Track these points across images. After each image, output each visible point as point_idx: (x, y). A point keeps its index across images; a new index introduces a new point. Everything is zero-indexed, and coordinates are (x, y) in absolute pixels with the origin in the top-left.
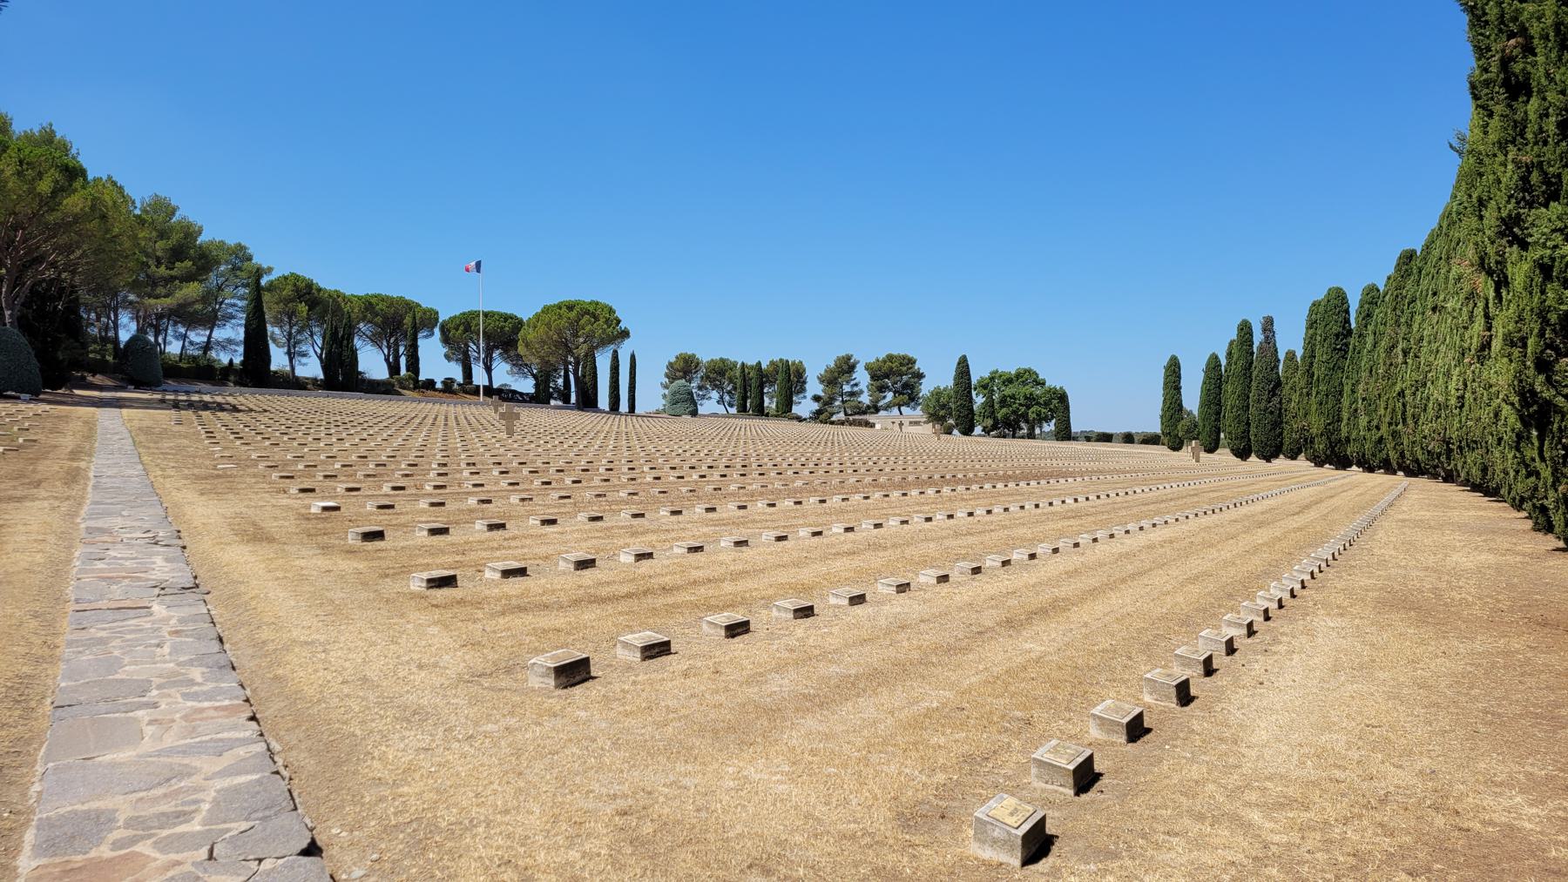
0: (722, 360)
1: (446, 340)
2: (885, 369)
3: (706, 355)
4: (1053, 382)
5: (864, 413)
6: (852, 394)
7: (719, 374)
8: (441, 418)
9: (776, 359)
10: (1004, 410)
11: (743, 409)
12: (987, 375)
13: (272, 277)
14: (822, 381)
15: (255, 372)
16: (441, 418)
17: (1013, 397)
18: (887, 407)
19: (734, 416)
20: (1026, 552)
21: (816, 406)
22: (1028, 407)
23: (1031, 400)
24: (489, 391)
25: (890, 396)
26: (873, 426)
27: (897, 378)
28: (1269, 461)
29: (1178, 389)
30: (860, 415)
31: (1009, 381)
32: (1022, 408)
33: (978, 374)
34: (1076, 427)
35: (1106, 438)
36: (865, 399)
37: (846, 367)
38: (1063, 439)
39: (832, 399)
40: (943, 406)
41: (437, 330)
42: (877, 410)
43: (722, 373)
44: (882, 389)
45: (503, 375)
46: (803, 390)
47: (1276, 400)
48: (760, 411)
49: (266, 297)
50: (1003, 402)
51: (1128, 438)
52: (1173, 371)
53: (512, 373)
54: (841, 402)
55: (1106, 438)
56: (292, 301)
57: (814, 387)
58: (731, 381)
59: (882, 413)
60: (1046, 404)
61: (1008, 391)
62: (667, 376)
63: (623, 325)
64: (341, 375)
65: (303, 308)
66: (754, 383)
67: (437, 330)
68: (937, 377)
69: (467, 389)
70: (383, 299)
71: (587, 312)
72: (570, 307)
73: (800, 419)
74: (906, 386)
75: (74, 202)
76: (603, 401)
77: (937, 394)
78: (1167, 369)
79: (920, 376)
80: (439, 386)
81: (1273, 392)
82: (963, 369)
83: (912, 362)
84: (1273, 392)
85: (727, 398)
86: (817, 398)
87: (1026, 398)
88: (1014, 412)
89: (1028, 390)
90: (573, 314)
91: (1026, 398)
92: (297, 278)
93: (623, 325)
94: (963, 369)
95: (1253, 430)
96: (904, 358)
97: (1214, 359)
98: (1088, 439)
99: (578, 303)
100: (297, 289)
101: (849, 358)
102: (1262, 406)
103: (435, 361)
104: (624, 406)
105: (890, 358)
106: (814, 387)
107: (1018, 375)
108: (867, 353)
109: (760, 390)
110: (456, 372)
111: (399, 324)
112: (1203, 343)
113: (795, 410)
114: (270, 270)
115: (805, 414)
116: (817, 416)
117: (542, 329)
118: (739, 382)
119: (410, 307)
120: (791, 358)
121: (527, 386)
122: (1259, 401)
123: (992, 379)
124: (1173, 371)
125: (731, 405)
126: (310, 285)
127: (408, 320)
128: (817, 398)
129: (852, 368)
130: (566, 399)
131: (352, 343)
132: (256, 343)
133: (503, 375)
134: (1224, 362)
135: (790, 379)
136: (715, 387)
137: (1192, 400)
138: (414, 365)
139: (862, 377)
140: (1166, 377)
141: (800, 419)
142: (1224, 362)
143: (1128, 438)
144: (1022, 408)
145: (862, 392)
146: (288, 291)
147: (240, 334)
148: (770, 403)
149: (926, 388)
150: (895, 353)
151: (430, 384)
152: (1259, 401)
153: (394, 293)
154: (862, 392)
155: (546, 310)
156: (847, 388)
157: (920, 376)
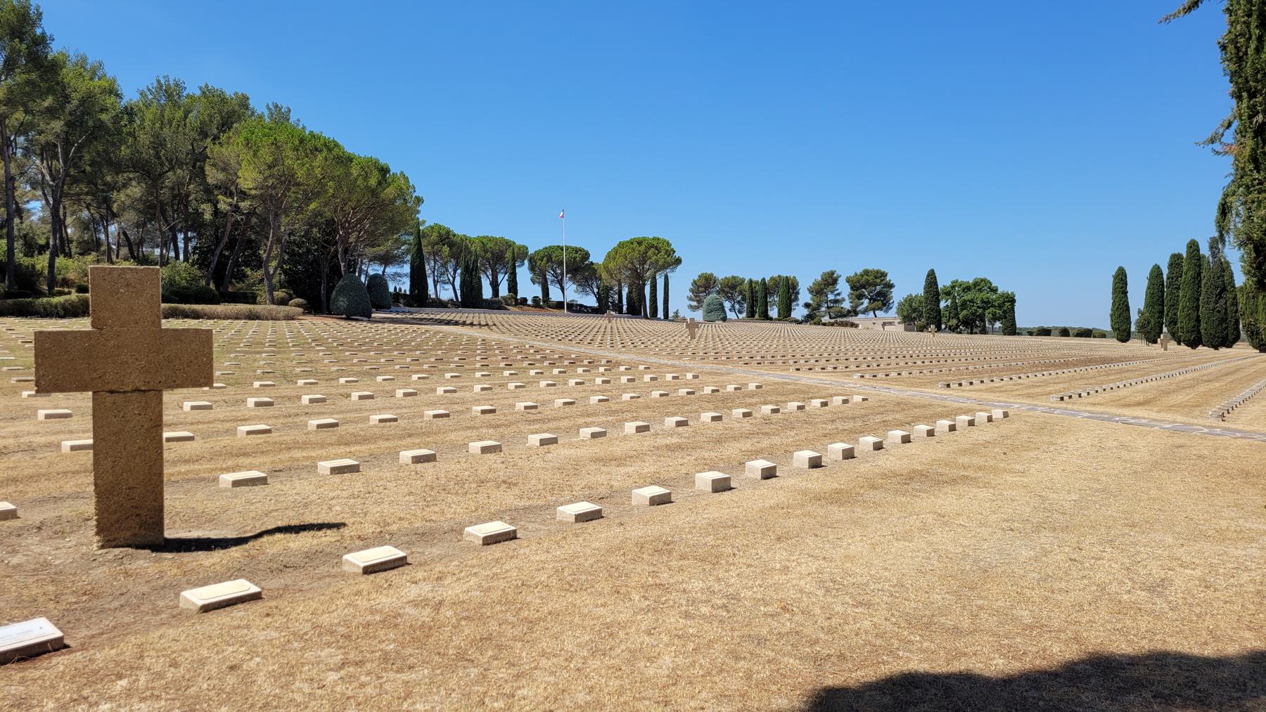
0: (733, 277)
1: (532, 269)
2: (863, 281)
3: (721, 274)
4: (1003, 287)
5: (845, 316)
6: (836, 301)
7: (731, 287)
8: (609, 329)
9: (775, 275)
10: (965, 312)
11: (751, 315)
12: (949, 284)
13: (427, 225)
14: (811, 292)
15: (418, 297)
16: (609, 329)
17: (972, 301)
18: (865, 311)
19: (743, 320)
20: (985, 415)
21: (806, 312)
22: (984, 309)
23: (987, 304)
24: (560, 305)
25: (866, 302)
26: (857, 326)
27: (873, 289)
28: (1216, 348)
29: (1125, 293)
30: (843, 318)
31: (967, 289)
32: (975, 310)
33: (943, 282)
34: (1020, 323)
35: (1045, 332)
36: (847, 305)
37: (830, 280)
38: (1010, 334)
39: (819, 306)
40: (915, 310)
41: (526, 262)
42: (856, 314)
43: (733, 287)
44: (860, 297)
45: (572, 293)
46: (796, 299)
47: (1222, 301)
48: (766, 317)
49: (424, 242)
50: (964, 305)
51: (1065, 332)
52: (1121, 280)
53: (576, 291)
54: (827, 307)
55: (1045, 332)
56: (437, 244)
57: (805, 297)
58: (740, 293)
59: (860, 316)
60: (1000, 307)
61: (968, 297)
62: (692, 291)
63: (677, 255)
64: (470, 298)
65: (446, 249)
66: (759, 295)
67: (526, 262)
68: (908, 286)
69: (543, 304)
70: (490, 239)
71: (652, 246)
72: (640, 243)
73: (797, 322)
74: (879, 294)
75: (390, 192)
76: (660, 314)
77: (910, 300)
78: (1115, 277)
79: (891, 286)
80: (530, 302)
81: (1220, 296)
82: (931, 279)
83: (884, 275)
84: (1220, 296)
85: (737, 306)
86: (807, 305)
87: (983, 302)
88: (973, 314)
89: (984, 295)
90: (642, 248)
91: (983, 302)
92: (440, 227)
93: (677, 255)
94: (931, 279)
95: (1203, 325)
96: (877, 272)
97: (1156, 272)
98: (1031, 333)
99: (645, 239)
100: (440, 235)
101: (833, 273)
102: (1211, 306)
103: (528, 289)
104: (660, 314)
105: (866, 272)
106: (805, 297)
107: (976, 284)
108: (847, 269)
109: (763, 300)
110: (537, 291)
111: (502, 256)
112: (1147, 254)
113: (794, 315)
114: (424, 222)
115: (800, 318)
116: (810, 318)
117: (620, 260)
118: (747, 294)
119: (509, 244)
120: (790, 274)
121: (591, 301)
122: (1208, 303)
123: (953, 287)
124: (1121, 280)
125: (740, 312)
126: (448, 232)
127: (508, 255)
128: (807, 305)
129: (835, 281)
130: (621, 312)
131: (481, 275)
132: (418, 277)
133: (572, 293)
134: (1165, 272)
135: (788, 289)
136: (728, 298)
137: (1137, 300)
138: (513, 287)
139: (844, 288)
140: (1115, 284)
141: (797, 322)
142: (1165, 272)
143: (1065, 332)
144: (975, 310)
145: (843, 300)
146: (434, 237)
147: (407, 269)
148: (774, 312)
149: (897, 296)
150: (870, 268)
151: (525, 300)
152: (1208, 303)
153: (497, 233)
154: (843, 300)
155: (621, 245)
156: (831, 297)
157: (891, 286)
